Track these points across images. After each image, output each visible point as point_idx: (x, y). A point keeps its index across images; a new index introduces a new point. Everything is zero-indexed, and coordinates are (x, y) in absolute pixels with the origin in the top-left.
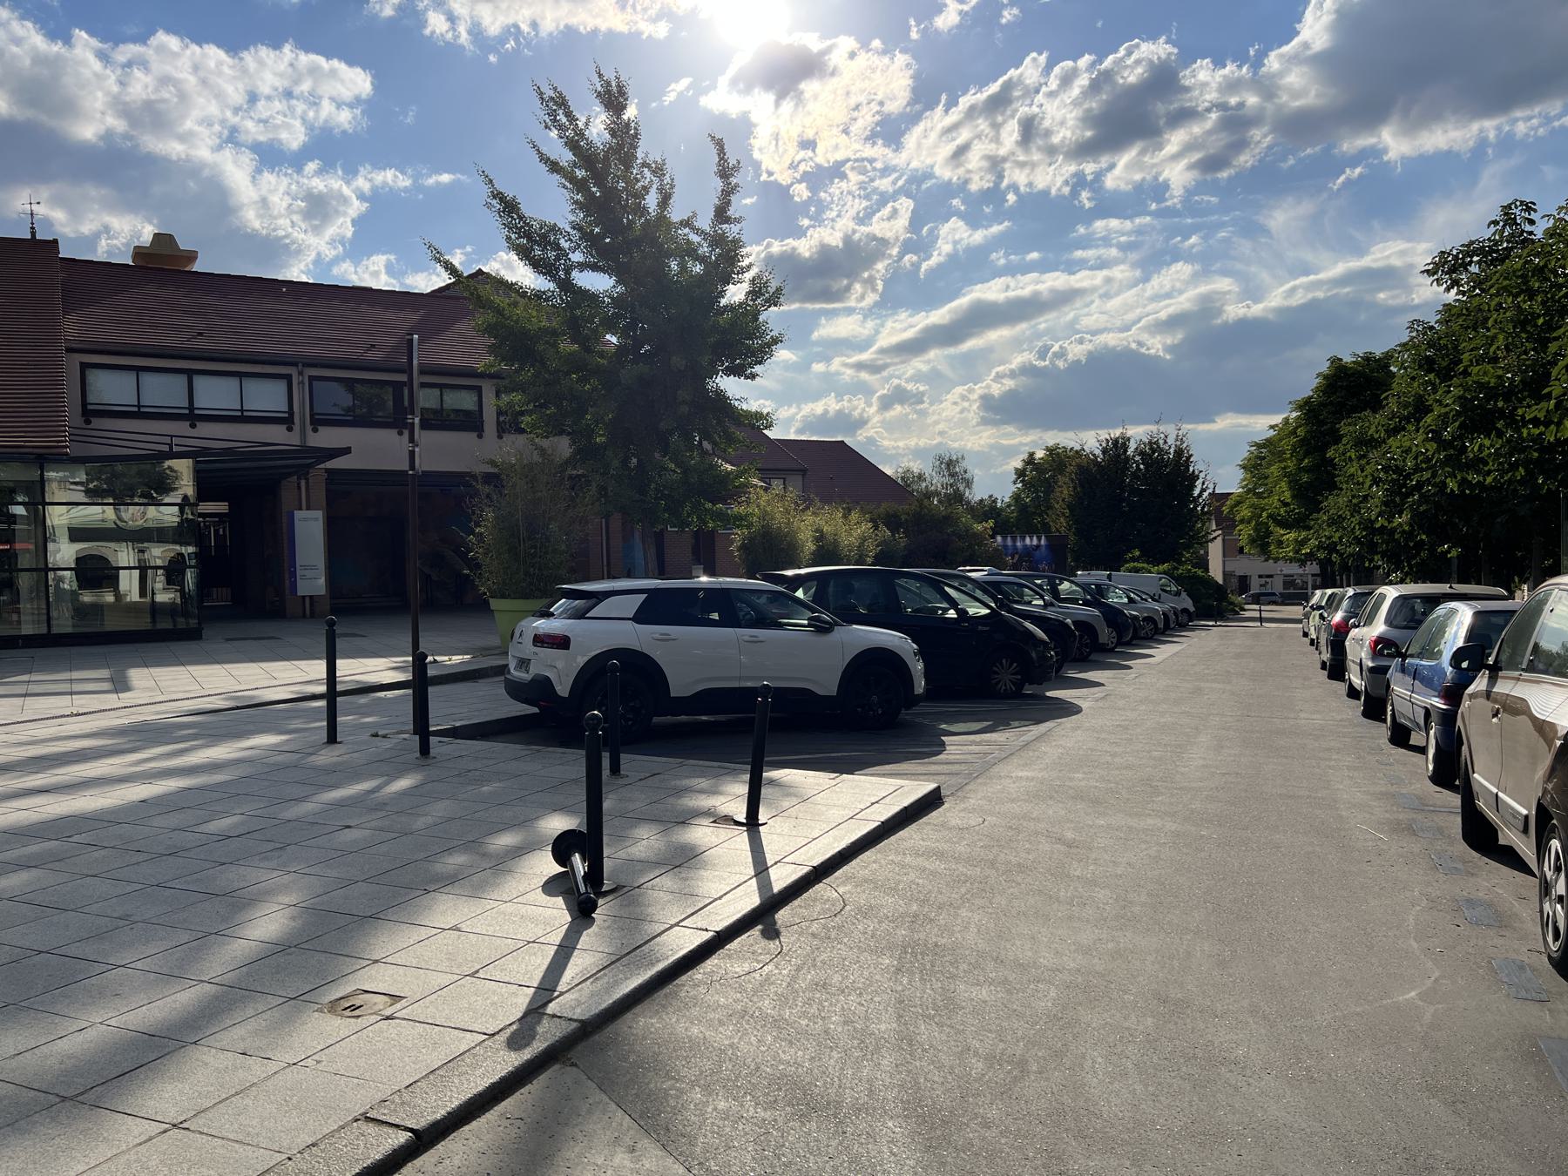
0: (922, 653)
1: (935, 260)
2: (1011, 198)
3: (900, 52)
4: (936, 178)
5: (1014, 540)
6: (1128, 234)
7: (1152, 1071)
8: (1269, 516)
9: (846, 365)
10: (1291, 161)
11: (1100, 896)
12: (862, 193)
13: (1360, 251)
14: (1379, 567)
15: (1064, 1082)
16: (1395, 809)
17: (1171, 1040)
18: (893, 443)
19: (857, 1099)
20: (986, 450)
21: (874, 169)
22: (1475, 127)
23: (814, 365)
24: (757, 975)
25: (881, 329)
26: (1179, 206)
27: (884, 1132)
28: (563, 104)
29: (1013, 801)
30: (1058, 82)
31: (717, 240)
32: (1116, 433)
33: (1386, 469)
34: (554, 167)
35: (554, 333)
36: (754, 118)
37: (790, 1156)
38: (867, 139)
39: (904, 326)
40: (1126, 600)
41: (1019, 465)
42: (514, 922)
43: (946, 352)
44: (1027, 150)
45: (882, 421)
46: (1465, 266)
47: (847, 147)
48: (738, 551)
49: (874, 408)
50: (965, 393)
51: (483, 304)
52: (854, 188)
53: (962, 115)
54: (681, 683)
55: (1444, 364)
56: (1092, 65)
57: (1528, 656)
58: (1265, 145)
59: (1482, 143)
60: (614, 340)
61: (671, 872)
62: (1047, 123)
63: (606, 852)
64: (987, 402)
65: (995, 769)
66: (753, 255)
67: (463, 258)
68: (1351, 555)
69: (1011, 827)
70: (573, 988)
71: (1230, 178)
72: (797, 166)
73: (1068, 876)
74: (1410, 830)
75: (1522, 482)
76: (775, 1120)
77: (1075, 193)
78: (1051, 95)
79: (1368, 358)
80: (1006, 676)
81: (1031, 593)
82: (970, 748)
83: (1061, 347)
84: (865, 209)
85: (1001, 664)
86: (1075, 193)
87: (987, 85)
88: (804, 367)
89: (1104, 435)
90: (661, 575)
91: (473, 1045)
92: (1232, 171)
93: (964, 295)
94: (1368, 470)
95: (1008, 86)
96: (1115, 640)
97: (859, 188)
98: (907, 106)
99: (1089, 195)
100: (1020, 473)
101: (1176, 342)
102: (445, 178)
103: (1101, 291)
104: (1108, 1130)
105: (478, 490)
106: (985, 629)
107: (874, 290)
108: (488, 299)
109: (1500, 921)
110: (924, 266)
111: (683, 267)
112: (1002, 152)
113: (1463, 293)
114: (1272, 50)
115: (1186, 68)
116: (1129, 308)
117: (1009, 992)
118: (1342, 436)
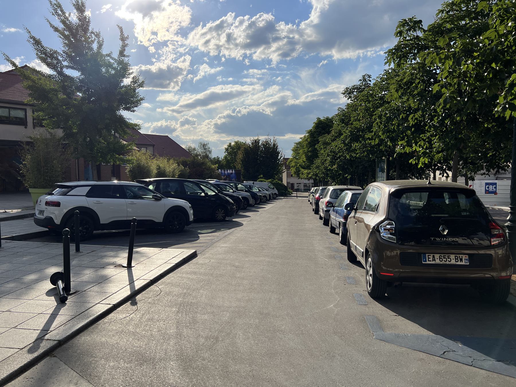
0: (193, 207)
1: (198, 77)
2: (223, 59)
3: (186, 6)
4: (199, 50)
5: (224, 171)
6: (260, 75)
7: (257, 336)
8: (300, 165)
9: (169, 110)
10: (307, 57)
11: (245, 282)
12: (174, 52)
13: (326, 86)
14: (329, 181)
15: (230, 343)
16: (330, 251)
17: (263, 326)
18: (185, 137)
19: (161, 356)
20: (216, 141)
21: (178, 45)
22: (357, 52)
23: (157, 109)
24: (128, 318)
25: (181, 99)
26: (275, 67)
27: (169, 366)
28: (60, 7)
29: (220, 254)
30: (238, 23)
31: (120, 63)
32: (256, 138)
33: (331, 152)
34: (56, 29)
35: (56, 91)
36: (135, 22)
37: (136, 379)
38: (175, 34)
39: (188, 98)
40: (258, 190)
41: (226, 147)
42: (33, 307)
43: (203, 108)
44: (229, 44)
45: (182, 130)
46: (353, 92)
47: (168, 36)
48: (128, 172)
49: (178, 125)
50: (209, 122)
51: (27, 78)
52: (171, 50)
53: (208, 30)
54: (104, 219)
55: (347, 121)
56: (249, 19)
57: (364, 206)
58: (300, 51)
59: (359, 57)
60: (81, 95)
61: (98, 285)
62: (235, 36)
63: (72, 279)
64: (216, 126)
65: (215, 244)
66: (134, 70)
67: (20, 61)
68: (322, 177)
69: (219, 263)
70: (56, 329)
71: (290, 60)
72: (151, 40)
73: (235, 277)
74: (334, 257)
75: (366, 156)
76: (131, 367)
77: (244, 60)
78: (236, 27)
79: (327, 119)
80: (220, 215)
81: (229, 188)
82: (208, 238)
83: (239, 109)
84: (175, 58)
85: (219, 211)
86: (244, 60)
87: (216, 21)
88: (154, 109)
89: (252, 138)
90: (99, 179)
91: (13, 353)
92: (290, 58)
93: (208, 90)
94: (326, 152)
95: (222, 22)
96: (254, 203)
97: (173, 51)
98: (189, 24)
99: (248, 61)
100: (227, 150)
101: (274, 110)
102: (13, 30)
103: (251, 92)
104: (242, 356)
105: (24, 147)
106: (213, 199)
107: (178, 85)
108: (28, 76)
109: (356, 282)
110: (195, 79)
111: (107, 71)
112: (221, 44)
113: (352, 100)
114: (302, 21)
115: (277, 24)
116: (260, 98)
117: (214, 316)
118: (319, 141)
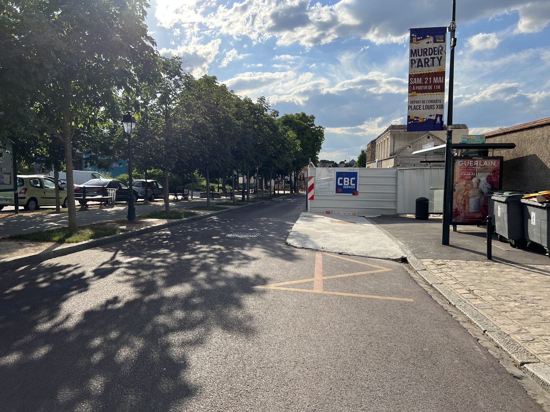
13: (367, 73)
103: (282, 80)
